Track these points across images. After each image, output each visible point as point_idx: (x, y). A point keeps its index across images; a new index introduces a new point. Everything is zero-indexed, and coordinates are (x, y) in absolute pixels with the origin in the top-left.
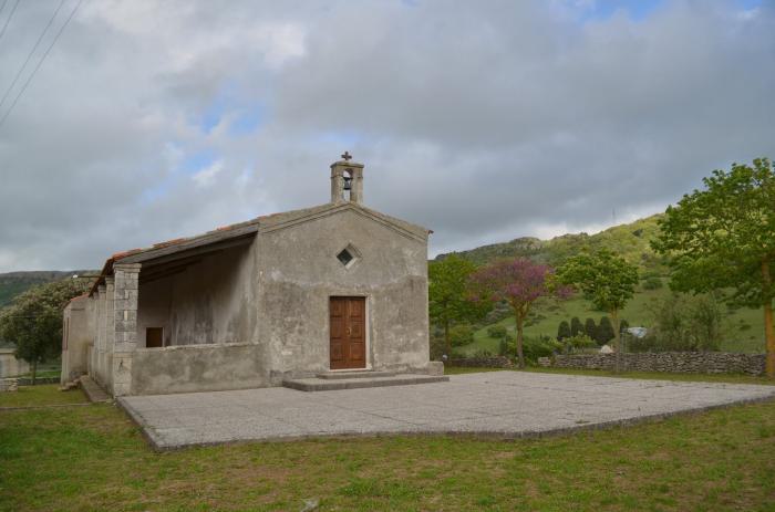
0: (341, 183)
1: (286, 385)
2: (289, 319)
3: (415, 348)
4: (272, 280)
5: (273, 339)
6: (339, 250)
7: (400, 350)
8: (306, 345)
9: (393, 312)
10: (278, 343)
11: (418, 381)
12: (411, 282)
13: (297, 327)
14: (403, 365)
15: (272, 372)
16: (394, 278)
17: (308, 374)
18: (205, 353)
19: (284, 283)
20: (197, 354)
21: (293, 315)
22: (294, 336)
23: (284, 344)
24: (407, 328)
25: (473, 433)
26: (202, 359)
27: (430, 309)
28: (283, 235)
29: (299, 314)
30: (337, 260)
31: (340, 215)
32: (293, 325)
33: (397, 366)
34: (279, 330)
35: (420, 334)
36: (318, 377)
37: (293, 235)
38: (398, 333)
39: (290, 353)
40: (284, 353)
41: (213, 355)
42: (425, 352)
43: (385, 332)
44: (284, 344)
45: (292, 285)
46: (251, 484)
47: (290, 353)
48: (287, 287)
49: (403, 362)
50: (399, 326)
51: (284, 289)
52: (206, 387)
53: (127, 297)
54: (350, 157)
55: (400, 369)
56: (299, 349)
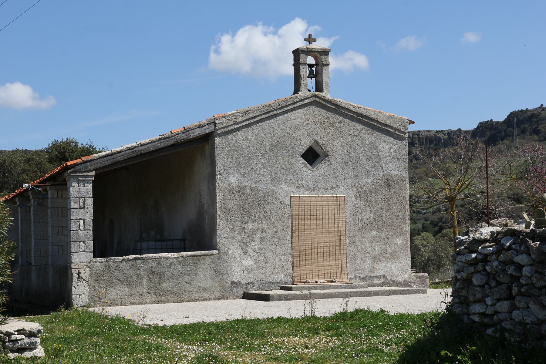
0: (304, 71)
1: (247, 296)
2: (250, 226)
3: (394, 257)
4: (230, 184)
5: (232, 248)
6: (303, 149)
7: (376, 259)
8: (269, 254)
9: (367, 214)
10: (238, 252)
11: (390, 293)
12: (388, 182)
13: (259, 234)
14: (379, 277)
15: (233, 283)
16: (368, 176)
17: (271, 285)
18: (163, 262)
19: (244, 187)
20: (154, 264)
21: (254, 221)
22: (253, 246)
23: (245, 253)
24: (383, 236)
25: (400, 294)
26: (160, 269)
27: (411, 206)
28: (240, 134)
29: (261, 220)
30: (302, 160)
31: (303, 110)
32: (254, 232)
33: (372, 278)
34: (238, 237)
35: (400, 242)
36: (282, 288)
37: (251, 133)
38: (372, 241)
39: (251, 263)
40: (244, 263)
41: (171, 265)
42: (406, 261)
43: (357, 239)
44: (245, 253)
45: (252, 189)
46: (65, 353)
47: (251, 263)
48: (247, 191)
49: (380, 273)
50: (374, 233)
51: (243, 193)
52: (163, 299)
53: (82, 205)
54: (315, 40)
55: (376, 281)
56: (261, 258)
